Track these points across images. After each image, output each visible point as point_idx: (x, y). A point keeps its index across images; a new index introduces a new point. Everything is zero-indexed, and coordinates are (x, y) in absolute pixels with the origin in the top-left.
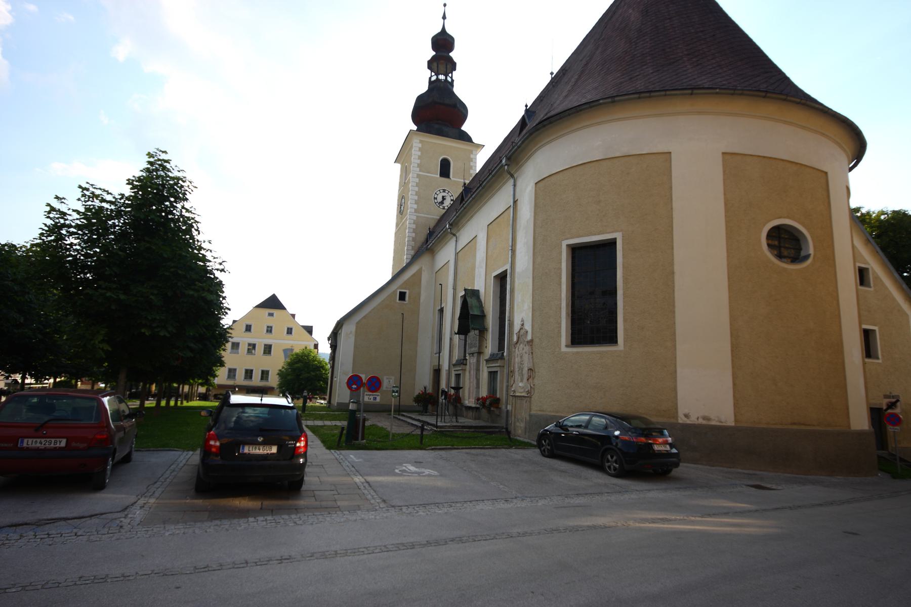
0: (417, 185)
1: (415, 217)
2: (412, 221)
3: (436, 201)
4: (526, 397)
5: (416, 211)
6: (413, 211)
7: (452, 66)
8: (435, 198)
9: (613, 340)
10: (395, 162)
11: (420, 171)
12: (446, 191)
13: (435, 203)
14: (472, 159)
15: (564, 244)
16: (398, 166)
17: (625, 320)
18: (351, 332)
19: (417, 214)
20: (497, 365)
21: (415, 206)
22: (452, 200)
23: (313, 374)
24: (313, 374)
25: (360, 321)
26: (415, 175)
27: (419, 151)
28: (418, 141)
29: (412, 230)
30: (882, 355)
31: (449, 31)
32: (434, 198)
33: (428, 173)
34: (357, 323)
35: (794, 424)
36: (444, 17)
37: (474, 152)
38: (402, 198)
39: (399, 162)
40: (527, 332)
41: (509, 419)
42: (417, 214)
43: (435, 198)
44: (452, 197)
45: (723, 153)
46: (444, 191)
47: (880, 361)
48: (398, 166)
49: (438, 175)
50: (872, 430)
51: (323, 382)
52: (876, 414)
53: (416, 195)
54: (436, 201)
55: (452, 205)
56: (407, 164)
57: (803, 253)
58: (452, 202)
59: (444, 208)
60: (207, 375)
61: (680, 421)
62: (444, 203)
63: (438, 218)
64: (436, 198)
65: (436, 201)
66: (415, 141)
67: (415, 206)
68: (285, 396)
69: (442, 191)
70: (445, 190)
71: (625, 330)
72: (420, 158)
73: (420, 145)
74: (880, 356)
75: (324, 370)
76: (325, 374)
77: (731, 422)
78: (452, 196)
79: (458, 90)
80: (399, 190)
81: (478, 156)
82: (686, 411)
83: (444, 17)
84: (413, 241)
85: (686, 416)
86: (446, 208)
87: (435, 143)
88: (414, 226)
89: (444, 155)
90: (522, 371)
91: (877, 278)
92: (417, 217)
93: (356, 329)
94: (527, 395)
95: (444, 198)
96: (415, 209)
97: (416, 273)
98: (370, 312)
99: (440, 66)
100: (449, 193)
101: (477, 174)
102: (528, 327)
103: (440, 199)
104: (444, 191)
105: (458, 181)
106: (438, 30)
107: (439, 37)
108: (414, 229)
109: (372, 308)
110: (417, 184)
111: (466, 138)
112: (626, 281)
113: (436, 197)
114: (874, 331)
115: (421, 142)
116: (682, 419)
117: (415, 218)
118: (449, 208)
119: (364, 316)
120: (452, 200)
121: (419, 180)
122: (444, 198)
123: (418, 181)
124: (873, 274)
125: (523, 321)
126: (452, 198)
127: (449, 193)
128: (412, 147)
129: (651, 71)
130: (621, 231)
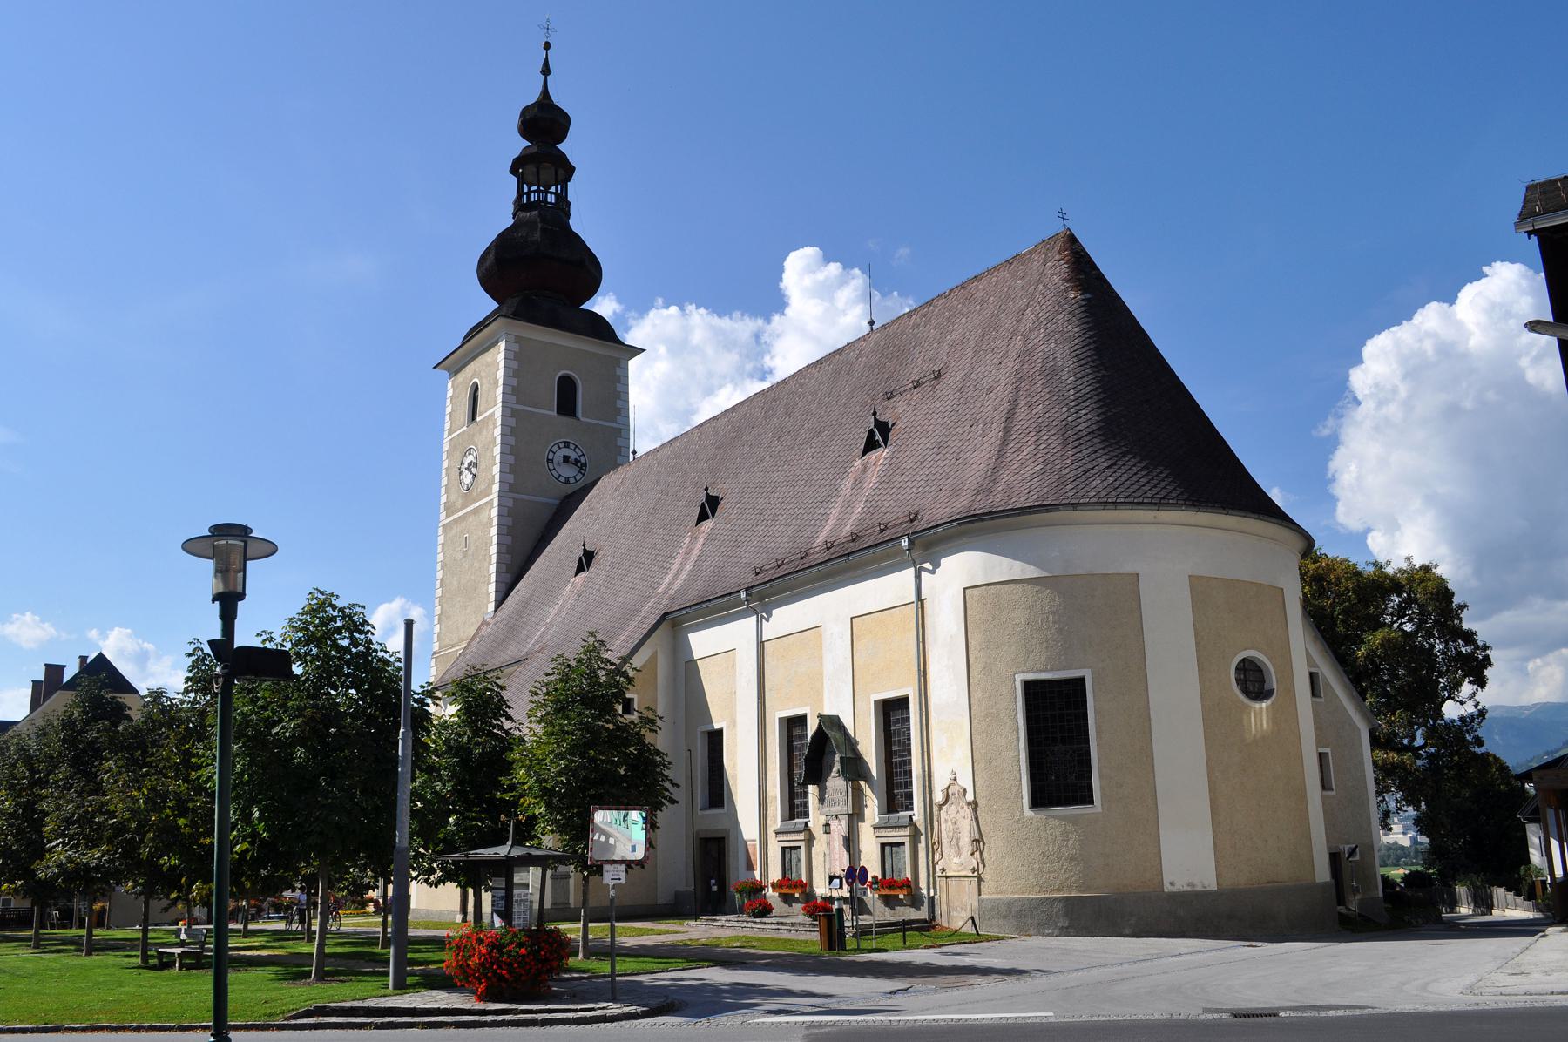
1: (512, 501)
4: (970, 877)
7: (565, 170)
9: (1089, 800)
12: (572, 446)
15: (1019, 678)
17: (1101, 777)
19: (516, 496)
20: (903, 834)
30: (1336, 785)
31: (558, 98)
32: (548, 459)
35: (1268, 882)
36: (546, 71)
40: (965, 791)
41: (937, 908)
42: (516, 496)
45: (1190, 576)
47: (1334, 793)
50: (1333, 881)
52: (1335, 858)
54: (551, 468)
57: (1267, 687)
61: (1166, 890)
63: (557, 502)
68: (553, 904)
69: (562, 445)
71: (1102, 788)
74: (1334, 787)
77: (1214, 887)
79: (579, 223)
82: (1171, 879)
83: (546, 71)
84: (508, 553)
85: (1171, 884)
90: (958, 840)
91: (1327, 684)
94: (971, 874)
99: (541, 172)
100: (577, 450)
102: (965, 781)
104: (567, 445)
106: (533, 97)
108: (508, 527)
111: (600, 329)
112: (1099, 731)
113: (550, 457)
114: (1327, 753)
116: (1167, 888)
124: (1323, 680)
125: (955, 774)
129: (1105, 464)
130: (1090, 667)
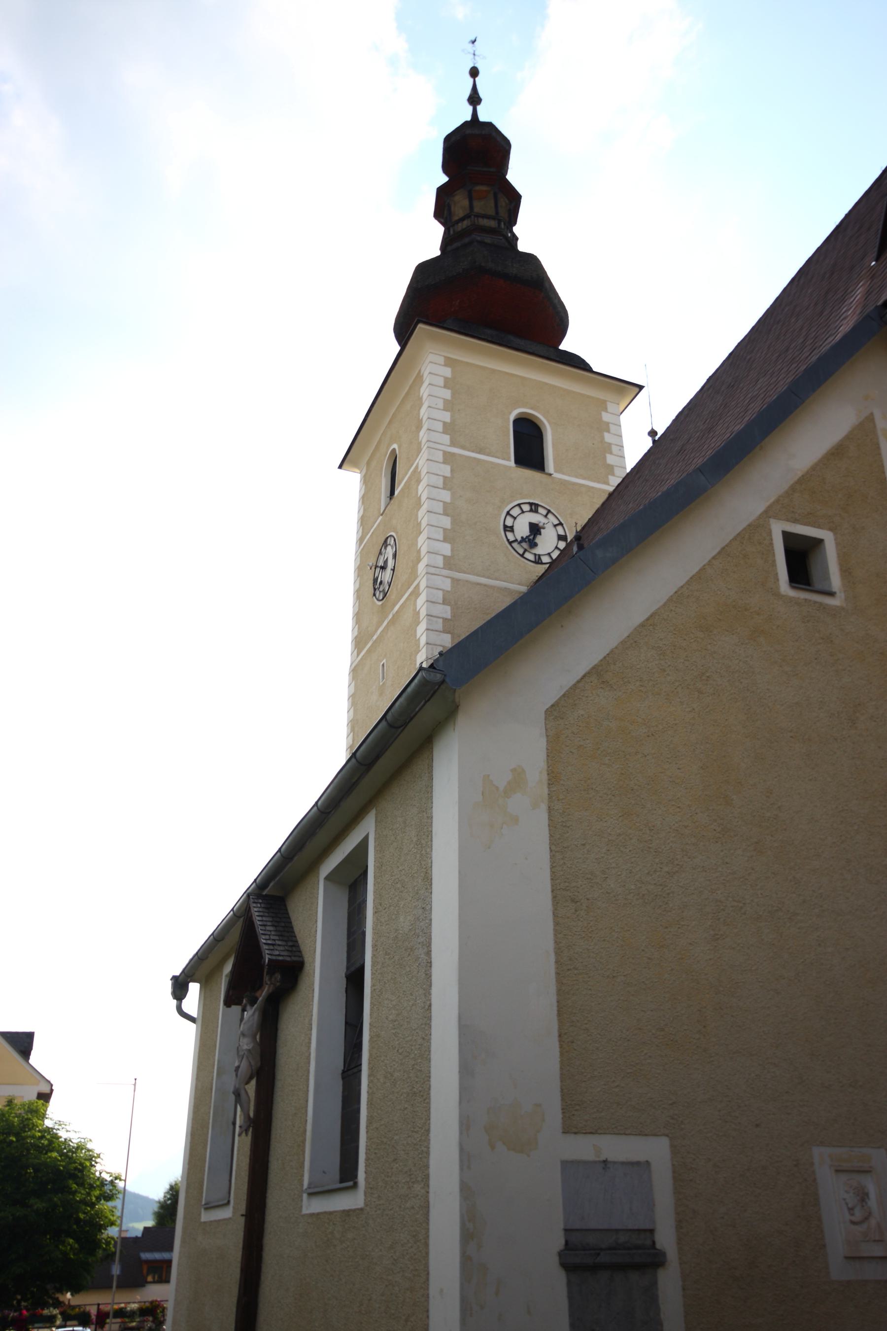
0: (447, 484)
1: (449, 581)
2: (440, 595)
3: (511, 537)
5: (449, 563)
6: (440, 561)
8: (508, 529)
10: (340, 467)
11: (453, 444)
12: (542, 511)
13: (510, 543)
14: (607, 424)
16: (353, 479)
18: (518, 779)
21: (446, 549)
22: (561, 538)
23: (38, 1204)
24: (38, 1204)
25: (572, 695)
26: (439, 456)
27: (446, 386)
28: (441, 360)
29: (439, 625)
32: (505, 527)
33: (480, 452)
34: (554, 712)
37: (611, 407)
38: (385, 544)
39: (355, 465)
43: (508, 529)
44: (560, 528)
46: (534, 508)
48: (353, 479)
49: (509, 460)
51: (77, 1240)
53: (445, 513)
55: (562, 551)
56: (395, 446)
58: (562, 545)
59: (538, 561)
60: (100, 1247)
62: (536, 545)
64: (511, 529)
65: (511, 537)
66: (431, 357)
67: (446, 549)
69: (526, 508)
70: (537, 505)
72: (448, 406)
73: (447, 372)
75: (81, 1184)
76: (84, 1202)
78: (561, 524)
80: (360, 540)
81: (626, 419)
86: (546, 559)
87: (493, 371)
88: (446, 611)
89: (524, 407)
92: (455, 581)
93: (553, 755)
95: (535, 529)
96: (445, 557)
97: (848, 437)
98: (630, 643)
101: (628, 474)
103: (522, 530)
104: (534, 508)
105: (574, 484)
107: (468, 131)
109: (639, 619)
110: (444, 483)
115: (449, 362)
117: (447, 585)
118: (553, 563)
119: (596, 671)
120: (561, 538)
121: (452, 471)
122: (535, 529)
123: (448, 474)
126: (561, 532)
127: (550, 516)
128: (419, 379)
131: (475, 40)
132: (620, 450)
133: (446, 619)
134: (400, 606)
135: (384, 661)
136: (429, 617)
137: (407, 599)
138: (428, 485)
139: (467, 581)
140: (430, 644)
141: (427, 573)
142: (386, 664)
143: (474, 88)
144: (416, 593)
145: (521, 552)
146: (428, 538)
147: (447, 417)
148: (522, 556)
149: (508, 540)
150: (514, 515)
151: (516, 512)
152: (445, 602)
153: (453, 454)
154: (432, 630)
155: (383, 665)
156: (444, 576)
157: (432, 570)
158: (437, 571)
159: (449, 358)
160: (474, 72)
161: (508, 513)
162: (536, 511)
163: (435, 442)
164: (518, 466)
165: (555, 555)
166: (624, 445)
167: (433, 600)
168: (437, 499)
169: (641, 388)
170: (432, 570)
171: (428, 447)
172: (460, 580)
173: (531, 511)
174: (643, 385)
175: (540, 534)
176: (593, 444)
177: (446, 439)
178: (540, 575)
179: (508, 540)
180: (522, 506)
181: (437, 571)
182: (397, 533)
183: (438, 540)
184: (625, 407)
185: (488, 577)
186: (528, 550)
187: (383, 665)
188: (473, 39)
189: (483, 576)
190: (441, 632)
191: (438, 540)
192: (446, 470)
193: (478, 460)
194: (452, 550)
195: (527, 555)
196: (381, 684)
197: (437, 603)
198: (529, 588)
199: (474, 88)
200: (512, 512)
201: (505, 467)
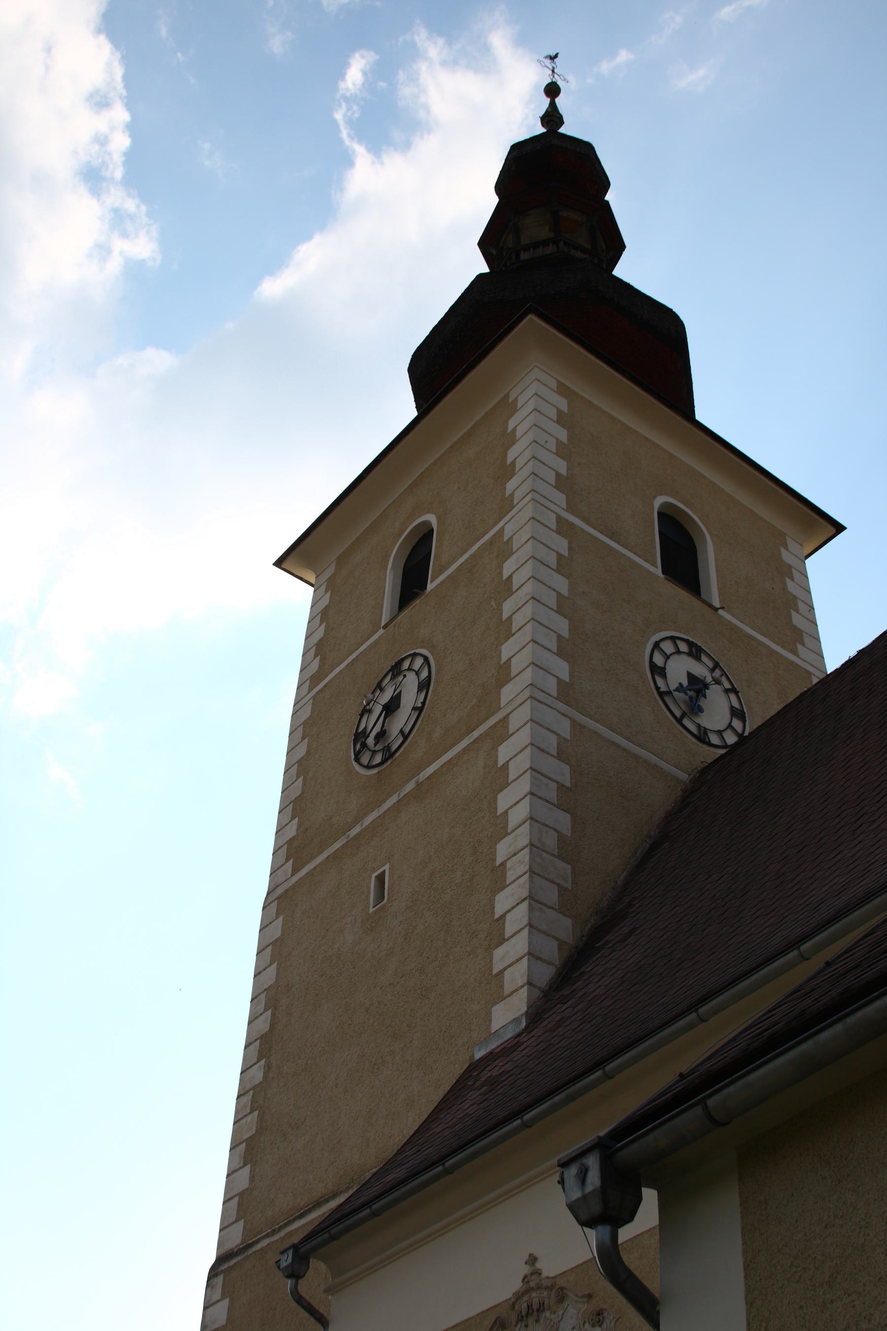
0: (563, 566)
8: (658, 671)
10: (279, 563)
11: (570, 509)
13: (661, 694)
56: (432, 518)
104: (695, 652)
115: (563, 390)
131: (556, 56)
132: (810, 610)
133: (563, 786)
134: (442, 766)
135: (387, 867)
136: (535, 774)
137: (466, 750)
138: (533, 557)
139: (596, 733)
140: (537, 821)
141: (531, 697)
142: (391, 877)
143: (553, 106)
144: (500, 733)
145: (678, 714)
146: (533, 641)
147: (562, 466)
148: (679, 721)
149: (657, 688)
150: (666, 652)
151: (668, 647)
152: (561, 755)
153: (572, 525)
154: (540, 798)
155: (381, 879)
156: (559, 712)
157: (541, 696)
158: (549, 701)
159: (563, 384)
160: (552, 90)
161: (657, 645)
162: (698, 659)
163: (544, 497)
164: (669, 578)
165: (731, 739)
166: (815, 607)
167: (543, 747)
168: (548, 584)
169: (839, 528)
170: (541, 696)
171: (533, 499)
172: (584, 727)
173: (690, 654)
174: (845, 525)
175: (705, 696)
176: (773, 588)
177: (561, 498)
178: (710, 761)
179: (657, 688)
180: (679, 643)
181: (549, 701)
182: (432, 648)
183: (549, 650)
184: (818, 545)
185: (628, 739)
186: (688, 714)
187: (381, 879)
188: (553, 54)
189: (620, 734)
190: (554, 805)
191: (549, 650)
192: (562, 545)
193: (611, 549)
194: (571, 674)
195: (686, 722)
196: (371, 910)
197: (548, 753)
198: (691, 777)
199: (553, 106)
200: (663, 645)
201: (651, 573)
